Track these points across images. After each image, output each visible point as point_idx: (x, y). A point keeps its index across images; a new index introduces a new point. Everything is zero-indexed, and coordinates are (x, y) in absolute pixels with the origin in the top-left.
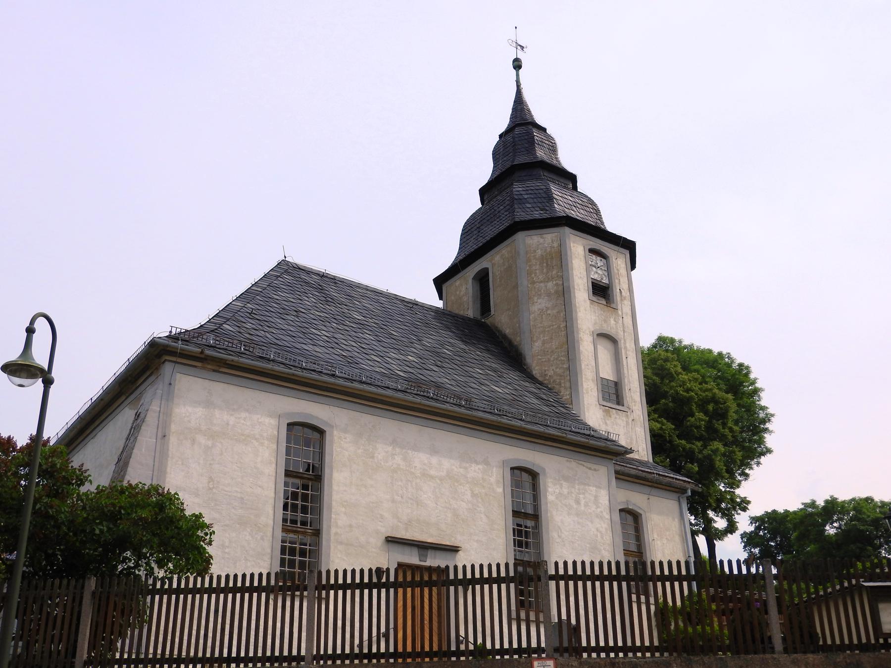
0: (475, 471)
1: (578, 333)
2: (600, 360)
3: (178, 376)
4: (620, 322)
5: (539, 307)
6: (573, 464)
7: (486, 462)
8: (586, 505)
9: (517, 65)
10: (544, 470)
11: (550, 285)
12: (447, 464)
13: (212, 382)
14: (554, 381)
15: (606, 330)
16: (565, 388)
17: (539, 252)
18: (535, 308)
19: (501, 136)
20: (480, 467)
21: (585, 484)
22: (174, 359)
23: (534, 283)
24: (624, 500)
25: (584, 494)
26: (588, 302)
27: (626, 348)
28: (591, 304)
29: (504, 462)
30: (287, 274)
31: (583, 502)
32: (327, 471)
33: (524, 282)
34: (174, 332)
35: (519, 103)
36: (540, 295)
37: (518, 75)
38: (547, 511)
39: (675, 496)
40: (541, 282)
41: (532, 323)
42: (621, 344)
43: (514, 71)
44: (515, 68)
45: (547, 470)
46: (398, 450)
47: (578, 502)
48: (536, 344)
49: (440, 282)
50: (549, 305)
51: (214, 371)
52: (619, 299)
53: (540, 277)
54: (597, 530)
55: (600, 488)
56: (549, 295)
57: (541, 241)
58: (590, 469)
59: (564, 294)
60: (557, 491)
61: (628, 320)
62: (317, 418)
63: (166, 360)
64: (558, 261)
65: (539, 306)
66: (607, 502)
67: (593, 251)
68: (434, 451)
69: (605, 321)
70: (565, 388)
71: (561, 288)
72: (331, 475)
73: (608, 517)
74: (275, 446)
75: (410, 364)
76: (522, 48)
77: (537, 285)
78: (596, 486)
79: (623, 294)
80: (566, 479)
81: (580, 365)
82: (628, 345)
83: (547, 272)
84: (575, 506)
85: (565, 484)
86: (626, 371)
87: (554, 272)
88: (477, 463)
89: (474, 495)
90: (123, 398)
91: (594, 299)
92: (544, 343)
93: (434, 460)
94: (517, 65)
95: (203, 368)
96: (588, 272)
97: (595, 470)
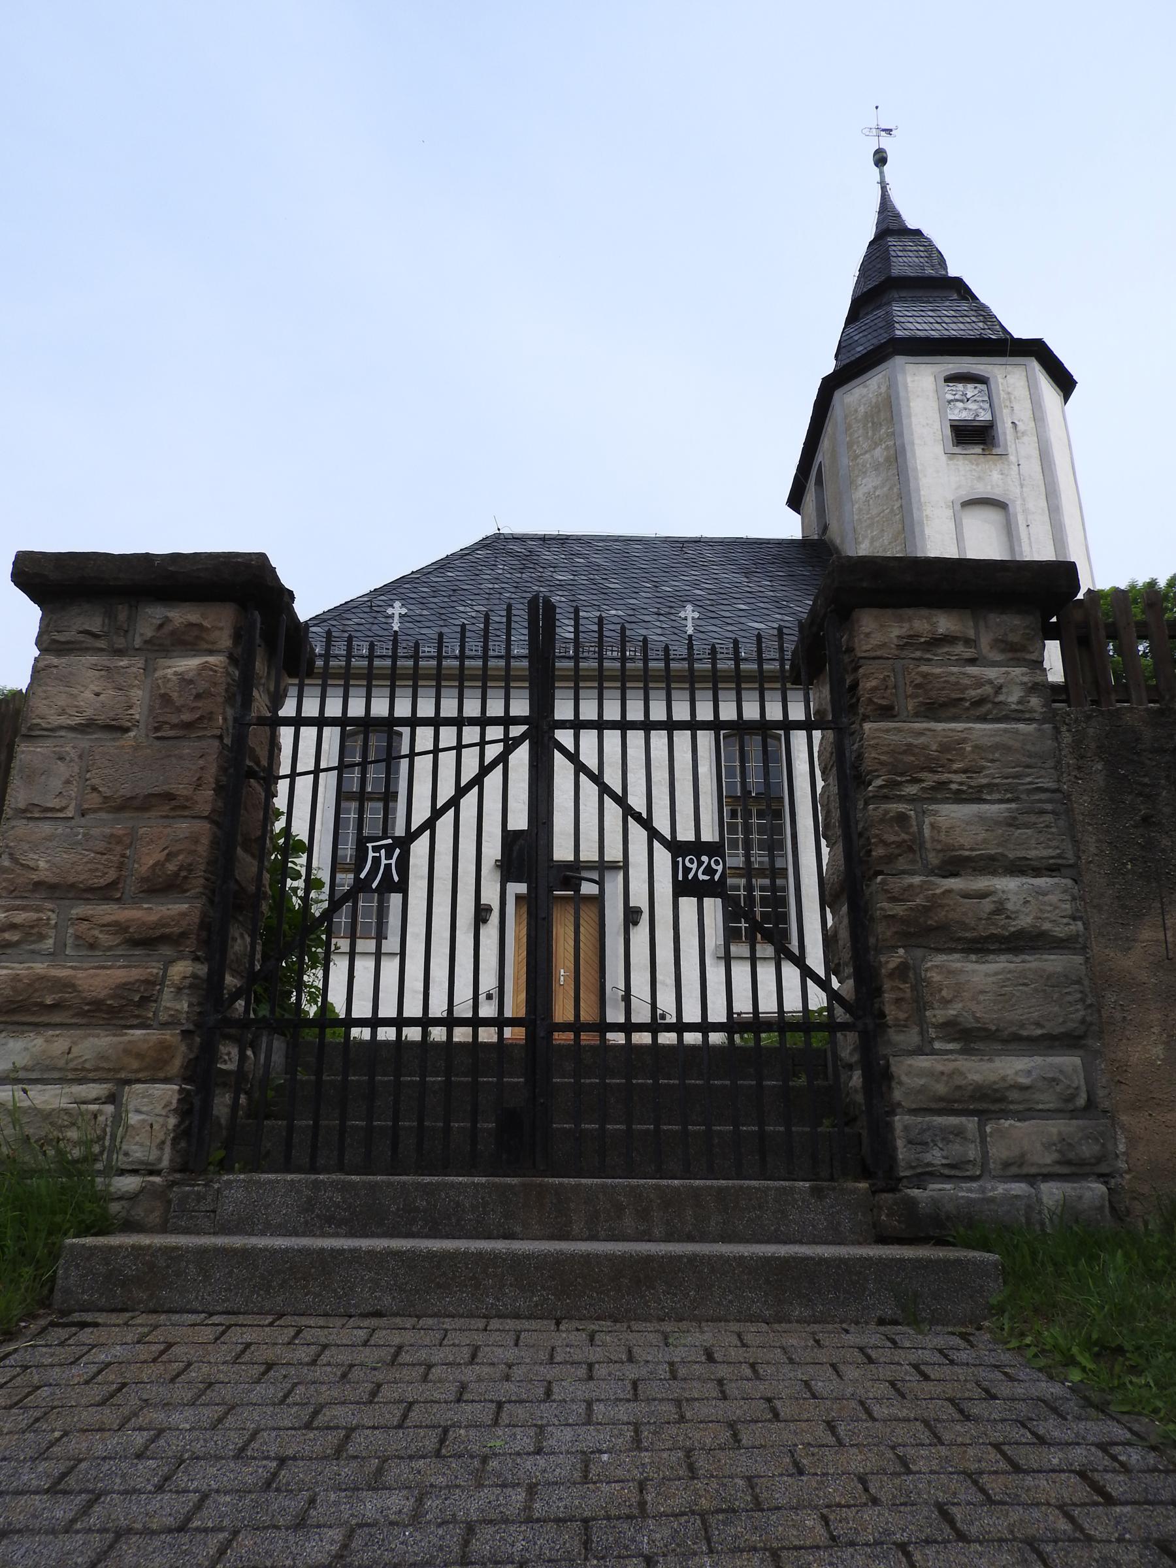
1: (920, 509)
5: (865, 490)
9: (880, 159)
15: (982, 491)
17: (862, 409)
18: (859, 494)
23: (856, 457)
26: (944, 458)
35: (887, 210)
36: (865, 473)
37: (882, 173)
40: (866, 452)
41: (856, 517)
42: (1016, 508)
43: (877, 170)
44: (876, 165)
48: (863, 546)
49: (795, 501)
50: (877, 482)
56: (877, 467)
57: (864, 391)
59: (897, 462)
61: (1032, 468)
64: (888, 413)
69: (980, 478)
71: (892, 452)
76: (888, 131)
79: (1021, 427)
82: (1031, 505)
83: (874, 434)
91: (957, 450)
92: (872, 541)
94: (880, 159)
96: (942, 412)
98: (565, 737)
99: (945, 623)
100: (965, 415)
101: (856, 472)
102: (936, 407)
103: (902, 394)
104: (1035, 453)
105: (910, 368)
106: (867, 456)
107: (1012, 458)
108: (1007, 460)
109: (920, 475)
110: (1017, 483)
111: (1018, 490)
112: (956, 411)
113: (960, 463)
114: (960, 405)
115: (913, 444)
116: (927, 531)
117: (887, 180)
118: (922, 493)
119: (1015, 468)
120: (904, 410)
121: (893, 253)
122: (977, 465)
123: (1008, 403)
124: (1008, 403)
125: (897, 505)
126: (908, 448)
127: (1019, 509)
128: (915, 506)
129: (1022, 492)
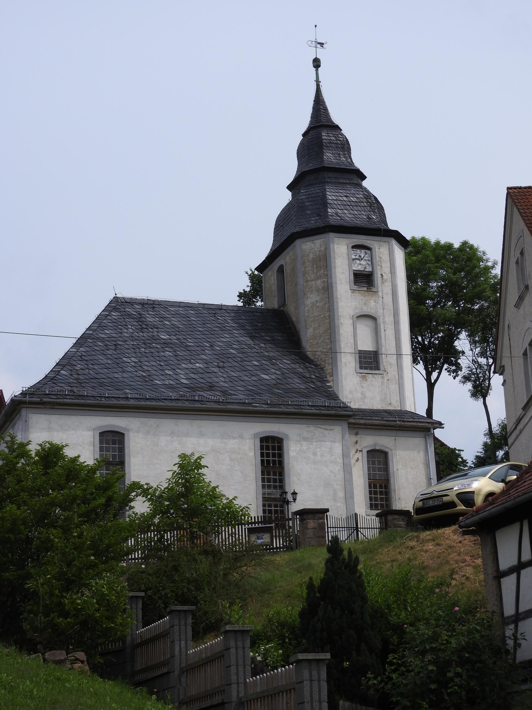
0: (232, 444)
1: (338, 320)
2: (359, 337)
3: (30, 415)
4: (380, 302)
6: (312, 428)
7: (241, 437)
8: (322, 455)
9: (317, 63)
10: (287, 436)
11: (319, 282)
12: (211, 442)
13: (50, 416)
14: (321, 359)
15: (366, 310)
16: (329, 364)
17: (311, 256)
18: (308, 302)
19: (304, 135)
20: (237, 440)
21: (322, 441)
22: (25, 406)
23: (307, 281)
24: (373, 443)
25: (320, 448)
27: (384, 322)
28: (352, 293)
29: (255, 435)
30: (118, 305)
31: (319, 454)
32: (127, 458)
33: (301, 281)
34: (24, 390)
37: (317, 74)
38: (289, 464)
39: (423, 434)
40: (313, 280)
41: (306, 314)
42: (380, 321)
44: (314, 67)
45: (290, 435)
46: (175, 438)
47: (315, 454)
48: (309, 331)
50: (318, 299)
51: (51, 408)
52: (380, 282)
53: (312, 276)
54: (331, 472)
55: (334, 442)
56: (318, 290)
57: (313, 245)
58: (326, 429)
59: (328, 290)
60: (298, 449)
61: (388, 299)
62: (118, 426)
63: (22, 407)
64: (324, 262)
65: (312, 299)
66: (341, 452)
67: (355, 247)
68: (201, 435)
69: (365, 304)
70: (329, 364)
71: (326, 285)
72: (130, 461)
73: (341, 461)
74: (92, 448)
75: (195, 371)
76: (322, 44)
77: (310, 283)
78: (332, 441)
79: (385, 277)
80: (305, 439)
81: (340, 345)
82: (387, 319)
84: (312, 457)
85: (304, 444)
86: (383, 342)
87: (322, 272)
88: (234, 438)
89: (231, 460)
90: (8, 423)
91: (355, 287)
93: (202, 441)
94: (317, 63)
95: (44, 408)
96: (350, 266)
97: (331, 430)
98: (359, 529)
99: (397, 517)
100: (360, 268)
101: (307, 289)
102: (347, 264)
103: (332, 255)
104: (390, 292)
105: (336, 240)
106: (313, 282)
107: (380, 294)
108: (378, 294)
109: (339, 301)
110: (381, 307)
111: (382, 312)
112: (356, 265)
113: (357, 295)
114: (358, 261)
115: (336, 283)
116: (341, 331)
117: (320, 79)
118: (339, 310)
119: (381, 299)
120: (333, 264)
121: (324, 144)
122: (364, 296)
123: (380, 263)
124: (380, 263)
125: (327, 314)
126: (334, 285)
127: (381, 321)
128: (336, 317)
129: (383, 312)
